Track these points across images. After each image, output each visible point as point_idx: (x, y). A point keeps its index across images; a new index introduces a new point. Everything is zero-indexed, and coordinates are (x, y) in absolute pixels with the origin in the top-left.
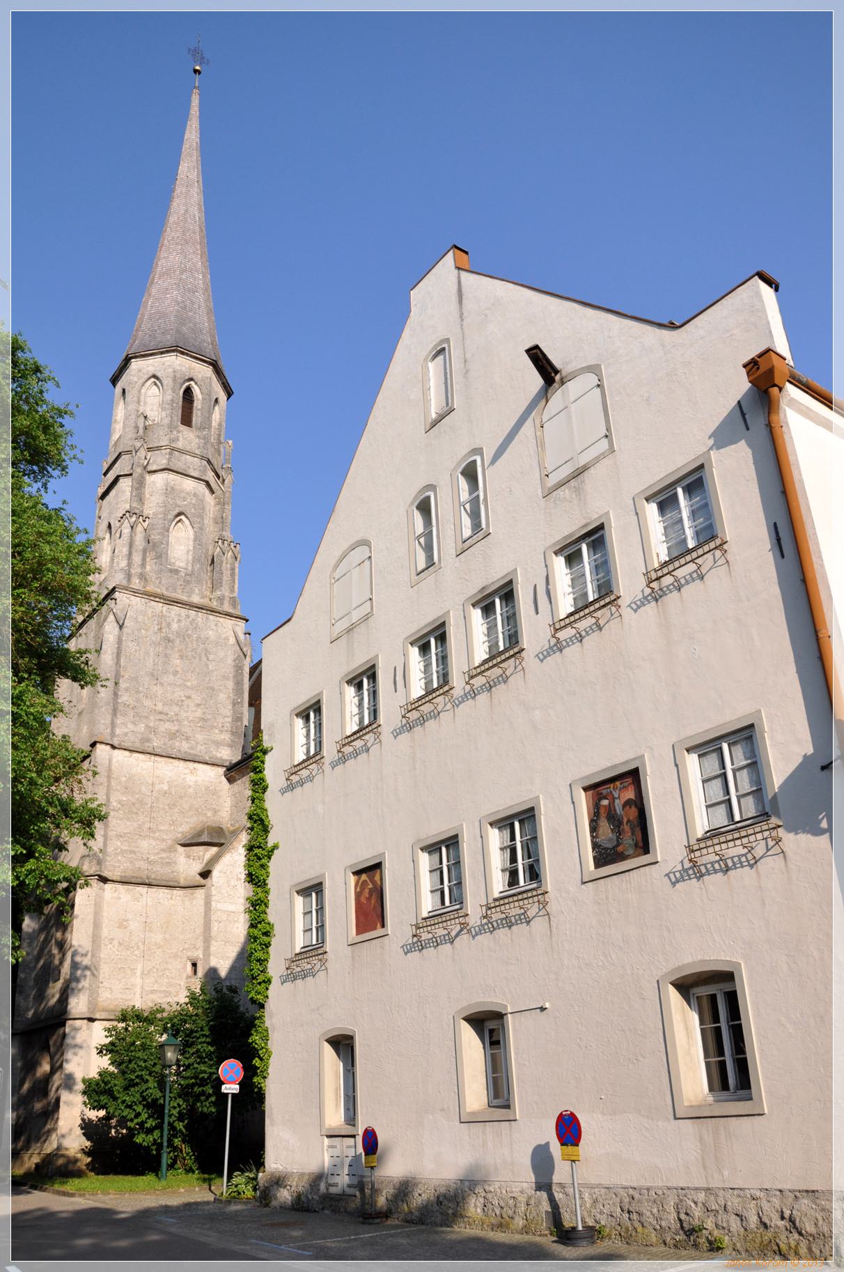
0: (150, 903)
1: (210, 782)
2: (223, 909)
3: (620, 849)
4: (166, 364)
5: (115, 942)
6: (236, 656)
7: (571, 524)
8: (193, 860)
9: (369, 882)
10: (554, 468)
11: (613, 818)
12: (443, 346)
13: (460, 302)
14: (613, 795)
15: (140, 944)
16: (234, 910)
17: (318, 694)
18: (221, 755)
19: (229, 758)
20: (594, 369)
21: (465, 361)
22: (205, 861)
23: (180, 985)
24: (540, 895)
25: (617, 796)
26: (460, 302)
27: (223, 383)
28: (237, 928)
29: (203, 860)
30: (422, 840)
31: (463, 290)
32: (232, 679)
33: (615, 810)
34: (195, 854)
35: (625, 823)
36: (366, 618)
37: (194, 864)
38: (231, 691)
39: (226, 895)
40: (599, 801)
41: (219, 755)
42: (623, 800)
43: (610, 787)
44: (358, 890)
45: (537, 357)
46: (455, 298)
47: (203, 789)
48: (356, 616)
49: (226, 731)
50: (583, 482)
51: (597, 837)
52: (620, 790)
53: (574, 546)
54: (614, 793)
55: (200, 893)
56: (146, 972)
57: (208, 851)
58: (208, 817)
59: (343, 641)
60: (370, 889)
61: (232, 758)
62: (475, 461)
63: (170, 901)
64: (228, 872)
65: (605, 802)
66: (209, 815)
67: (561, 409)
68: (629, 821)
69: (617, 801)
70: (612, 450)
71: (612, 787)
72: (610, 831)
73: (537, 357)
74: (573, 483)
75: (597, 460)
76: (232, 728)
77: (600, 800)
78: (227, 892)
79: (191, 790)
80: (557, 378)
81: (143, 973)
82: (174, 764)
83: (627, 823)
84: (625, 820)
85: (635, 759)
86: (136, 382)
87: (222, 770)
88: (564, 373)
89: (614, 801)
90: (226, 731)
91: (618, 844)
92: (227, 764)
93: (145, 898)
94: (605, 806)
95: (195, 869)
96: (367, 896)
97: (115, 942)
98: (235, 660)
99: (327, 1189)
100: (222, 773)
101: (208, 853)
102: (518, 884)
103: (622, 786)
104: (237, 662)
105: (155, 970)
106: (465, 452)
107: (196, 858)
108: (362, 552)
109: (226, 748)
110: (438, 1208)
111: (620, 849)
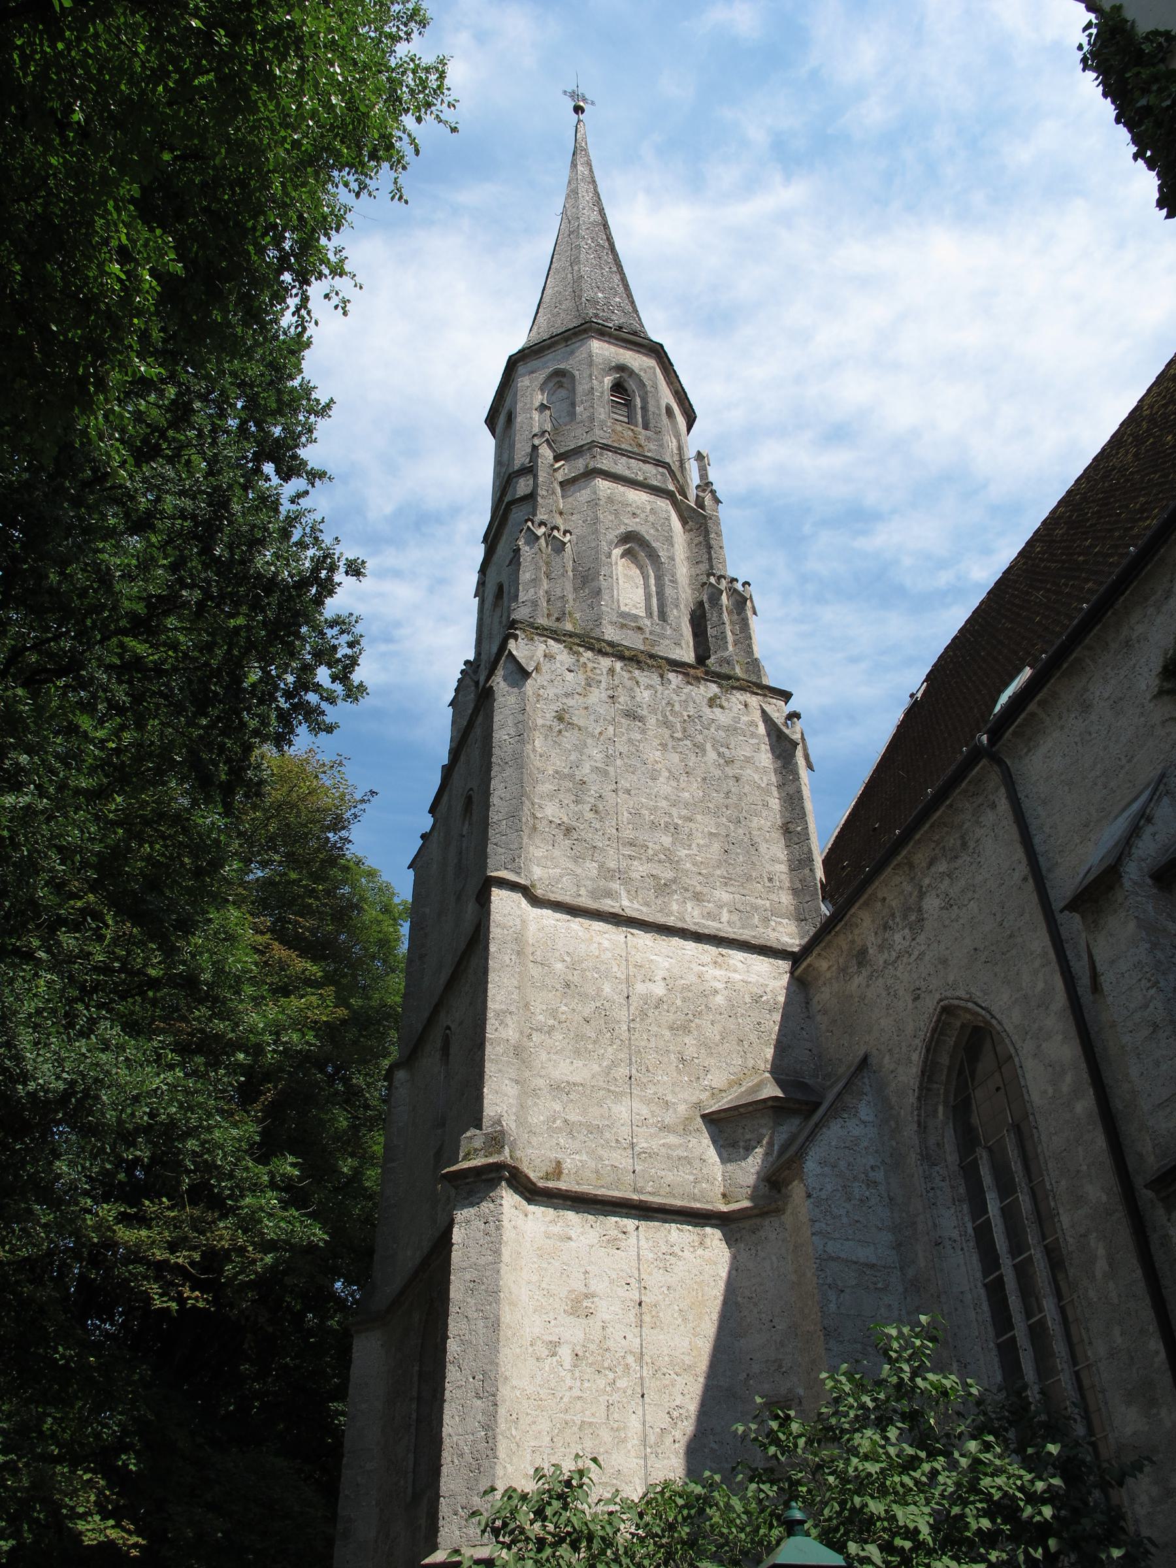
5: (565, 1353)
15: (630, 1359)
22: (776, 1147)
34: (748, 1137)
39: (845, 1220)
47: (748, 1000)
63: (700, 1252)
76: (791, 881)
97: (565, 1353)
109: (785, 921)
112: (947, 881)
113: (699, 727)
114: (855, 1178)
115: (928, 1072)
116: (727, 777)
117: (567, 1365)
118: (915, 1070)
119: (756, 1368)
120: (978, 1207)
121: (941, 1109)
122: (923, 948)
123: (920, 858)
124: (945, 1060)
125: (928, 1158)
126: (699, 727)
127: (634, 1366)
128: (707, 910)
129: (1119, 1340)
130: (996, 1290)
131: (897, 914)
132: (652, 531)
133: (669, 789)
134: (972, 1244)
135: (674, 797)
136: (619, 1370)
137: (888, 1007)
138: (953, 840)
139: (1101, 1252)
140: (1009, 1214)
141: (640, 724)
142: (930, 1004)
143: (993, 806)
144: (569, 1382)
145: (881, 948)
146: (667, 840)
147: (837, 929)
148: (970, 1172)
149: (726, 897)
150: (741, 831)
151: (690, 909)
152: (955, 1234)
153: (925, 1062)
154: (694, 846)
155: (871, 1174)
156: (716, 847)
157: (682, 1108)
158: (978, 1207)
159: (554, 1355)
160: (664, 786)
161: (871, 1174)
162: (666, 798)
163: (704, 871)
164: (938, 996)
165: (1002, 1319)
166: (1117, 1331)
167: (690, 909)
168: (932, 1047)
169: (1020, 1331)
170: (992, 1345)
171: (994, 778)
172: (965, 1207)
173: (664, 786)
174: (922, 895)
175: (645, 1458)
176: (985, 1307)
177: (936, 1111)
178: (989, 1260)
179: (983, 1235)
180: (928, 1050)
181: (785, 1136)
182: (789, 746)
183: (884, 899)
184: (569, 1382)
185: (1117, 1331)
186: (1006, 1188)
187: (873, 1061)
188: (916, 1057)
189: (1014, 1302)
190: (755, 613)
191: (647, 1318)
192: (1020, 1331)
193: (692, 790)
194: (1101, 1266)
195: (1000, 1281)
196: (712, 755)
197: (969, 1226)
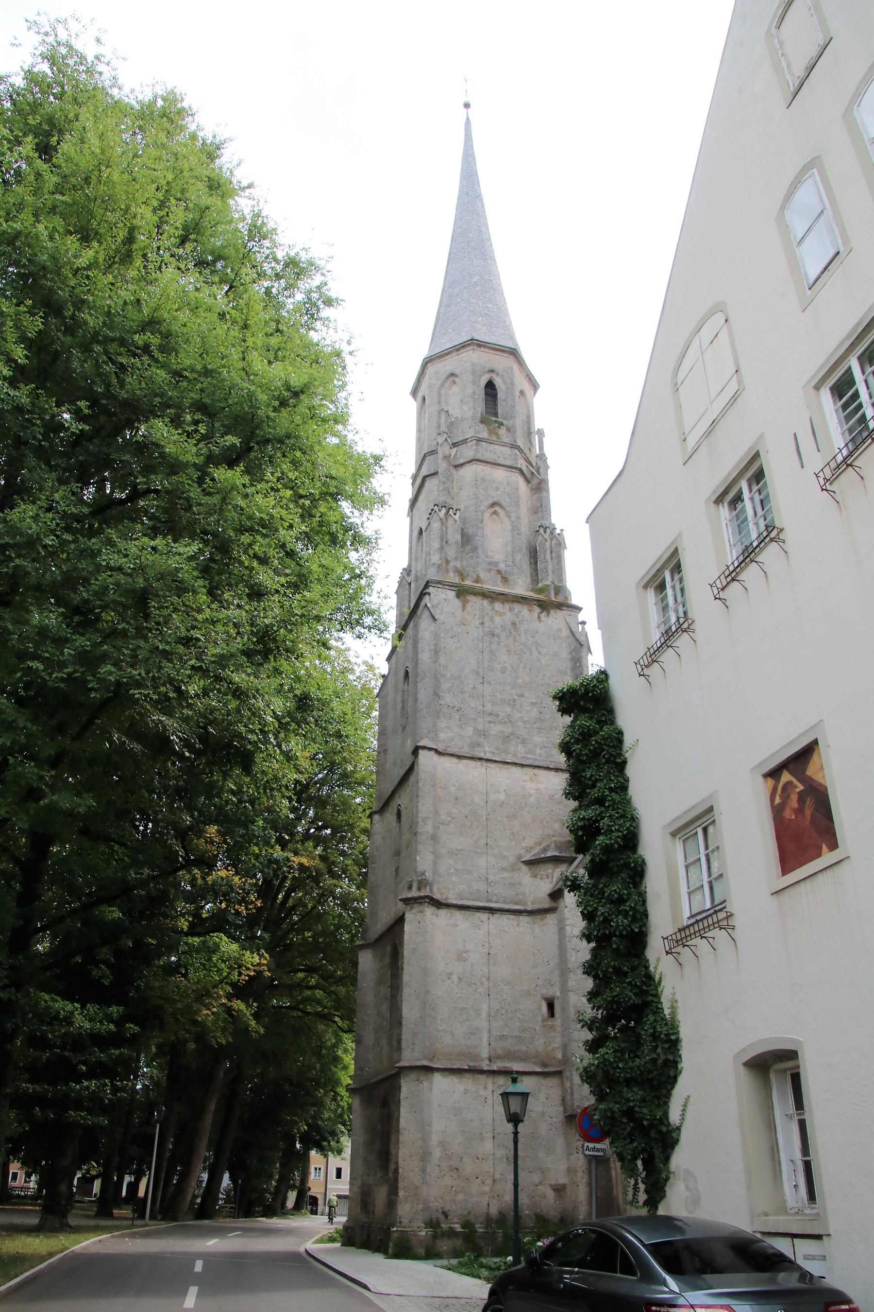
5: (455, 978)
15: (484, 980)
44: (778, 800)
55: (551, 920)
56: (493, 1014)
58: (554, 830)
60: (799, 793)
81: (489, 1015)
93: (486, 925)
97: (455, 978)
104: (574, 654)
117: (456, 983)
127: (486, 982)
136: (478, 985)
144: (456, 990)
159: (449, 979)
184: (456, 990)
191: (491, 961)
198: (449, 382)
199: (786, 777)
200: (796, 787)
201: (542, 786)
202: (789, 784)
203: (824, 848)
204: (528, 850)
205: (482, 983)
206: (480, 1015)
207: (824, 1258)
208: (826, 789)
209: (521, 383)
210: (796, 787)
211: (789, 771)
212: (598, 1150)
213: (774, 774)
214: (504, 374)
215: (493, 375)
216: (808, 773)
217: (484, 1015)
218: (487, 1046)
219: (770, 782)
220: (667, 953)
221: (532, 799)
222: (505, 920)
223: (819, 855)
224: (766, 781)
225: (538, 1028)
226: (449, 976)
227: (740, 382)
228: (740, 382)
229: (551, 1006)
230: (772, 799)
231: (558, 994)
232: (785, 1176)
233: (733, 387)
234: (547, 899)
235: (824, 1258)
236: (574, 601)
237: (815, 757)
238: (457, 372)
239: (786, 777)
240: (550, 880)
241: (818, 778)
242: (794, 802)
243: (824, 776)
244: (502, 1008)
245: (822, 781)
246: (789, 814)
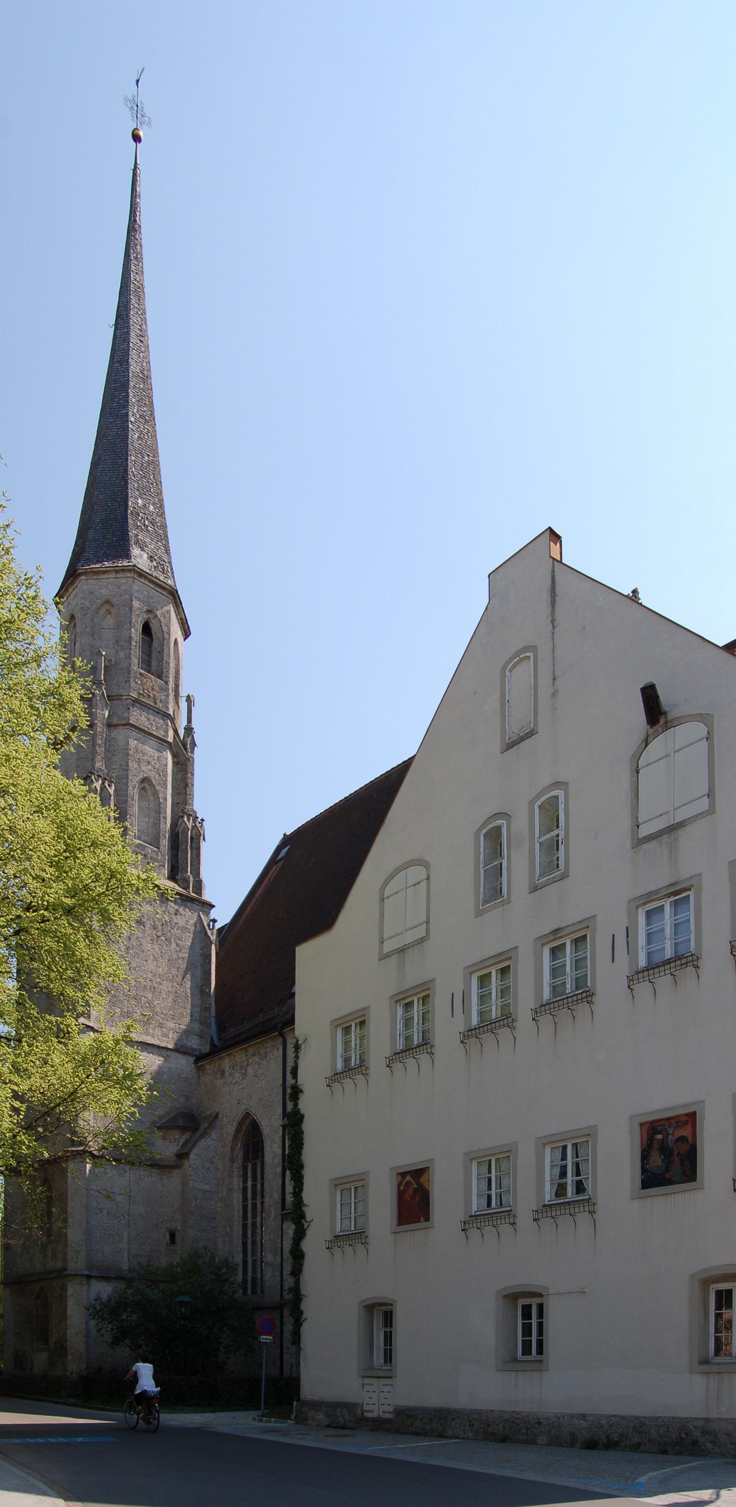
0: (133, 1179)
1: (182, 1070)
2: (199, 1188)
3: (667, 1175)
4: (122, 588)
5: (105, 1212)
6: (204, 944)
7: (659, 879)
8: (170, 1142)
9: (413, 1182)
10: (647, 819)
11: (664, 1149)
12: (528, 654)
13: (553, 604)
14: (667, 1131)
15: (125, 1214)
16: (209, 1189)
17: (364, 1009)
18: (191, 1044)
19: (198, 1048)
20: (705, 718)
21: (554, 679)
22: (181, 1144)
23: (161, 1251)
24: (590, 1205)
25: (671, 1132)
26: (553, 604)
27: (181, 619)
28: (211, 1205)
29: (179, 1143)
30: (473, 1152)
31: (558, 589)
32: (199, 968)
33: (668, 1144)
34: (171, 1137)
35: (675, 1155)
36: (421, 941)
37: (170, 1147)
38: (199, 980)
39: (201, 1176)
40: (654, 1136)
41: (189, 1044)
42: (676, 1137)
43: (665, 1125)
44: (402, 1188)
45: (650, 695)
46: (546, 597)
47: (176, 1076)
48: (410, 937)
49: (195, 1020)
50: (676, 840)
51: (648, 1163)
52: (675, 1128)
53: (657, 902)
54: (668, 1129)
55: (176, 1173)
56: (132, 1239)
57: (183, 1135)
58: (180, 1103)
59: (394, 958)
60: (415, 1188)
61: (201, 1048)
62: (557, 797)
63: (150, 1178)
64: (203, 1155)
65: (659, 1137)
66: (181, 1101)
67: (661, 756)
68: (679, 1154)
69: (670, 1137)
70: (711, 811)
71: (667, 1124)
72: (660, 1160)
73: (650, 695)
74: (665, 838)
75: (694, 819)
76: (200, 1017)
77: (654, 1134)
78: (202, 1173)
79: (165, 1076)
80: (662, 721)
81: (129, 1240)
82: (149, 1050)
83: (677, 1155)
84: (676, 1152)
85: (695, 1103)
86: (88, 608)
87: (192, 1059)
88: (670, 717)
89: (667, 1137)
90: (195, 1020)
91: (667, 1171)
92: (197, 1053)
93: (128, 1174)
94: (659, 1140)
95: (172, 1150)
96: (411, 1194)
97: (105, 1212)
98: (202, 949)
99: (363, 1414)
100: (193, 1061)
101: (183, 1137)
102: (566, 1195)
103: (677, 1125)
104: (205, 950)
105: (139, 1238)
106: (547, 782)
107: (172, 1140)
108: (416, 873)
109: (195, 1037)
110: (469, 1428)
111: (667, 1175)
112: (257, 1066)
113: (169, 928)
114: (207, 1161)
115: (238, 1130)
116: (179, 958)
117: (105, 1216)
118: (234, 1129)
119: (166, 1219)
120: (245, 1181)
121: (240, 1144)
122: (245, 1086)
123: (251, 1051)
124: (244, 1128)
125: (232, 1160)
126: (169, 928)
127: (127, 1217)
128: (163, 1032)
129: (272, 1237)
130: (245, 1208)
131: (238, 1066)
132: (157, 776)
133: (153, 967)
134: (241, 1191)
135: (155, 971)
136: (122, 1218)
137: (229, 1100)
138: (262, 1051)
139: (274, 1212)
140: (254, 1187)
141: (142, 927)
142: (243, 1108)
143: (278, 1050)
144: (106, 1221)
145: (230, 1074)
146: (150, 996)
147: (216, 1058)
148: (245, 1168)
149: (172, 1025)
150: (182, 990)
151: (157, 1032)
152: (236, 1187)
153: (237, 1127)
154: (161, 999)
155: (213, 1159)
156: (170, 999)
157: (147, 1124)
158: (245, 1181)
159: (101, 1212)
160: (151, 965)
161: (213, 1159)
162: (151, 972)
163: (164, 1012)
164: (246, 1108)
165: (245, 1217)
166: (272, 1234)
167: (157, 1032)
168: (240, 1123)
169: (250, 1221)
170: (241, 1223)
171: (280, 1040)
172: (241, 1179)
173: (151, 965)
174: (248, 1065)
175: (129, 1244)
176: (241, 1212)
177: (238, 1144)
178: (245, 1199)
179: (245, 1189)
180: (239, 1123)
181: (184, 1139)
182: (209, 942)
183: (235, 1056)
184: (106, 1221)
185: (272, 1234)
186: (254, 1179)
187: (220, 1117)
188: (235, 1124)
189: (250, 1214)
190: (204, 839)
191: (131, 1201)
192: (250, 1221)
193: (163, 969)
194: (272, 1216)
195: (247, 1205)
196: (174, 945)
197: (241, 1185)
198: (103, 610)
199: (408, 1178)
200: (413, 1185)
201: (173, 1066)
202: (408, 1182)
203: (422, 1219)
204: (160, 1118)
205: (124, 1217)
206: (123, 1239)
207: (392, 1385)
208: (429, 1192)
209: (176, 631)
210: (413, 1185)
211: (411, 1175)
212: (268, 1340)
213: (403, 1175)
214: (162, 619)
215: (151, 616)
216: (421, 1180)
217: (125, 1239)
218: (127, 1262)
219: (400, 1178)
220: (327, 1248)
221: (165, 1076)
222: (142, 1171)
223: (419, 1222)
224: (397, 1176)
225: (163, 1250)
226: (101, 1210)
227: (428, 931)
228: (428, 931)
229: (173, 1236)
230: (399, 1186)
231: (179, 1228)
232: (375, 1354)
233: (421, 932)
234: (174, 1158)
235: (392, 1385)
236: (207, 896)
237: (426, 1174)
238: (114, 600)
239: (408, 1178)
240: (177, 1143)
241: (426, 1185)
242: (411, 1191)
243: (429, 1185)
244: (138, 1235)
245: (427, 1187)
246: (407, 1197)
